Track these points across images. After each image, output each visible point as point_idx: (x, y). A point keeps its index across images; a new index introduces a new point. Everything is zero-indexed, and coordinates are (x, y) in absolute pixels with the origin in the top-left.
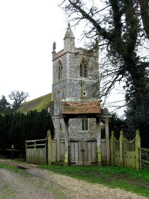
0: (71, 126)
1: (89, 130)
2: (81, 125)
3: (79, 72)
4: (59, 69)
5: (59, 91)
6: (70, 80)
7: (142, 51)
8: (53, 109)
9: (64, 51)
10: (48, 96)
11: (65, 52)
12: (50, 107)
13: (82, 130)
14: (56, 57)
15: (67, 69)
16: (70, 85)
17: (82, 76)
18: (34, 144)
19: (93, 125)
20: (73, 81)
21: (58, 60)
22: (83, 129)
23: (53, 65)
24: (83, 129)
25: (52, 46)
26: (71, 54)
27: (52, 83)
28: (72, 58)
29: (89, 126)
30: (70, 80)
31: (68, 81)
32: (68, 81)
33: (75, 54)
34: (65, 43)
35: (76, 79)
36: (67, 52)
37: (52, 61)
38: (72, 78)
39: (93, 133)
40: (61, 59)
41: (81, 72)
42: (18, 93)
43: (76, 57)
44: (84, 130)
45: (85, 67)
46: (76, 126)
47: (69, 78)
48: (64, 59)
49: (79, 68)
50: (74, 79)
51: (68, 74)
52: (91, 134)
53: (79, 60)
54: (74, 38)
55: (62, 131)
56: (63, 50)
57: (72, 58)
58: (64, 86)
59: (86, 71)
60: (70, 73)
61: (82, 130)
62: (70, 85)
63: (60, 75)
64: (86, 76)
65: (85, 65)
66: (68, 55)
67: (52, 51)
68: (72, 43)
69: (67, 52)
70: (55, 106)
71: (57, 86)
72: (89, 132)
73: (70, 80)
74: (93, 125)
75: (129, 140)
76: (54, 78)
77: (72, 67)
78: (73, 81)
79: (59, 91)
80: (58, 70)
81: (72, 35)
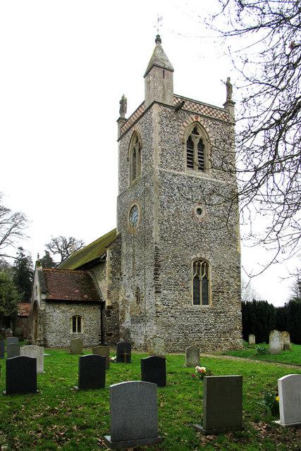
0: (165, 292)
1: (211, 302)
2: (192, 292)
3: (185, 156)
4: (134, 154)
5: (134, 206)
6: (162, 175)
7: (269, 191)
8: (119, 253)
9: (145, 104)
10: (113, 232)
11: (147, 105)
12: (112, 247)
13: (194, 304)
14: (132, 133)
15: (153, 146)
16: (160, 187)
17: (192, 167)
18: (43, 293)
19: (223, 292)
20: (170, 177)
21: (130, 133)
22: (196, 302)
23: (120, 148)
24: (196, 302)
25: (118, 106)
26: (163, 108)
27: (117, 193)
28: (166, 117)
29: (211, 293)
30: (161, 172)
31: (157, 177)
32: (157, 177)
33: (174, 110)
34: (148, 83)
35: (176, 173)
36: (153, 104)
37: (118, 141)
38: (167, 170)
39: (220, 313)
40: (138, 127)
41: (190, 157)
42: (65, 241)
43: (178, 118)
44: (199, 304)
45: (201, 146)
46: (177, 292)
47: (157, 168)
48: (145, 124)
49: (185, 146)
50: (172, 171)
51: (156, 160)
52: (218, 314)
53: (186, 125)
54: (172, 71)
55: (140, 305)
56: (143, 103)
57: (166, 117)
58: (147, 190)
59: (201, 156)
60: (162, 155)
61: (194, 304)
62: (160, 187)
63: (137, 168)
64: (202, 168)
65: (201, 140)
66: (156, 109)
67: (119, 116)
68: (166, 80)
69: (153, 104)
70: (124, 245)
71: (130, 197)
72: (212, 310)
73: (161, 172)
74: (223, 292)
75: (105, 302)
76: (122, 180)
77: (167, 142)
78: (170, 177)
79: (133, 207)
80: (131, 156)
81: (166, 63)
